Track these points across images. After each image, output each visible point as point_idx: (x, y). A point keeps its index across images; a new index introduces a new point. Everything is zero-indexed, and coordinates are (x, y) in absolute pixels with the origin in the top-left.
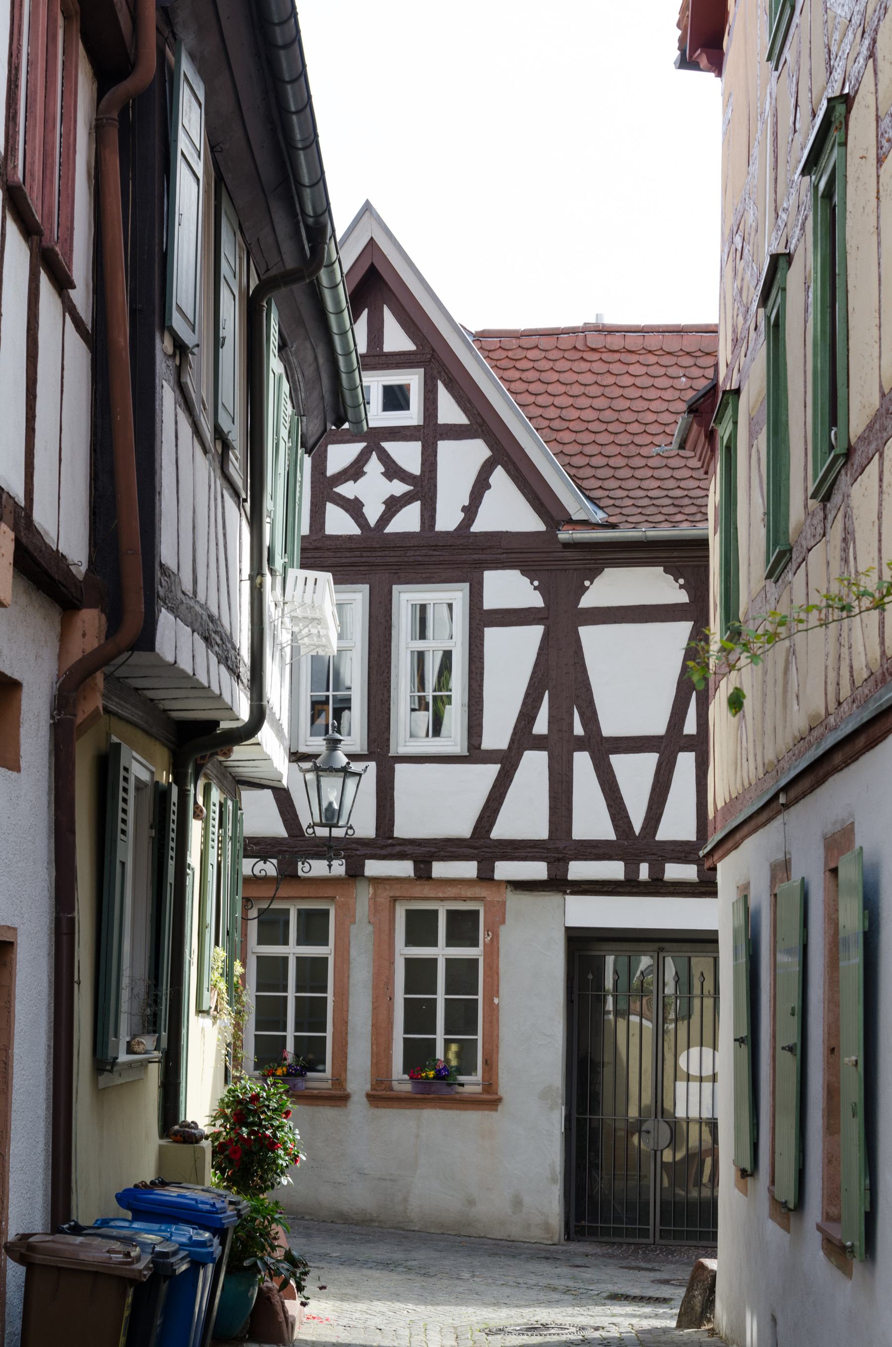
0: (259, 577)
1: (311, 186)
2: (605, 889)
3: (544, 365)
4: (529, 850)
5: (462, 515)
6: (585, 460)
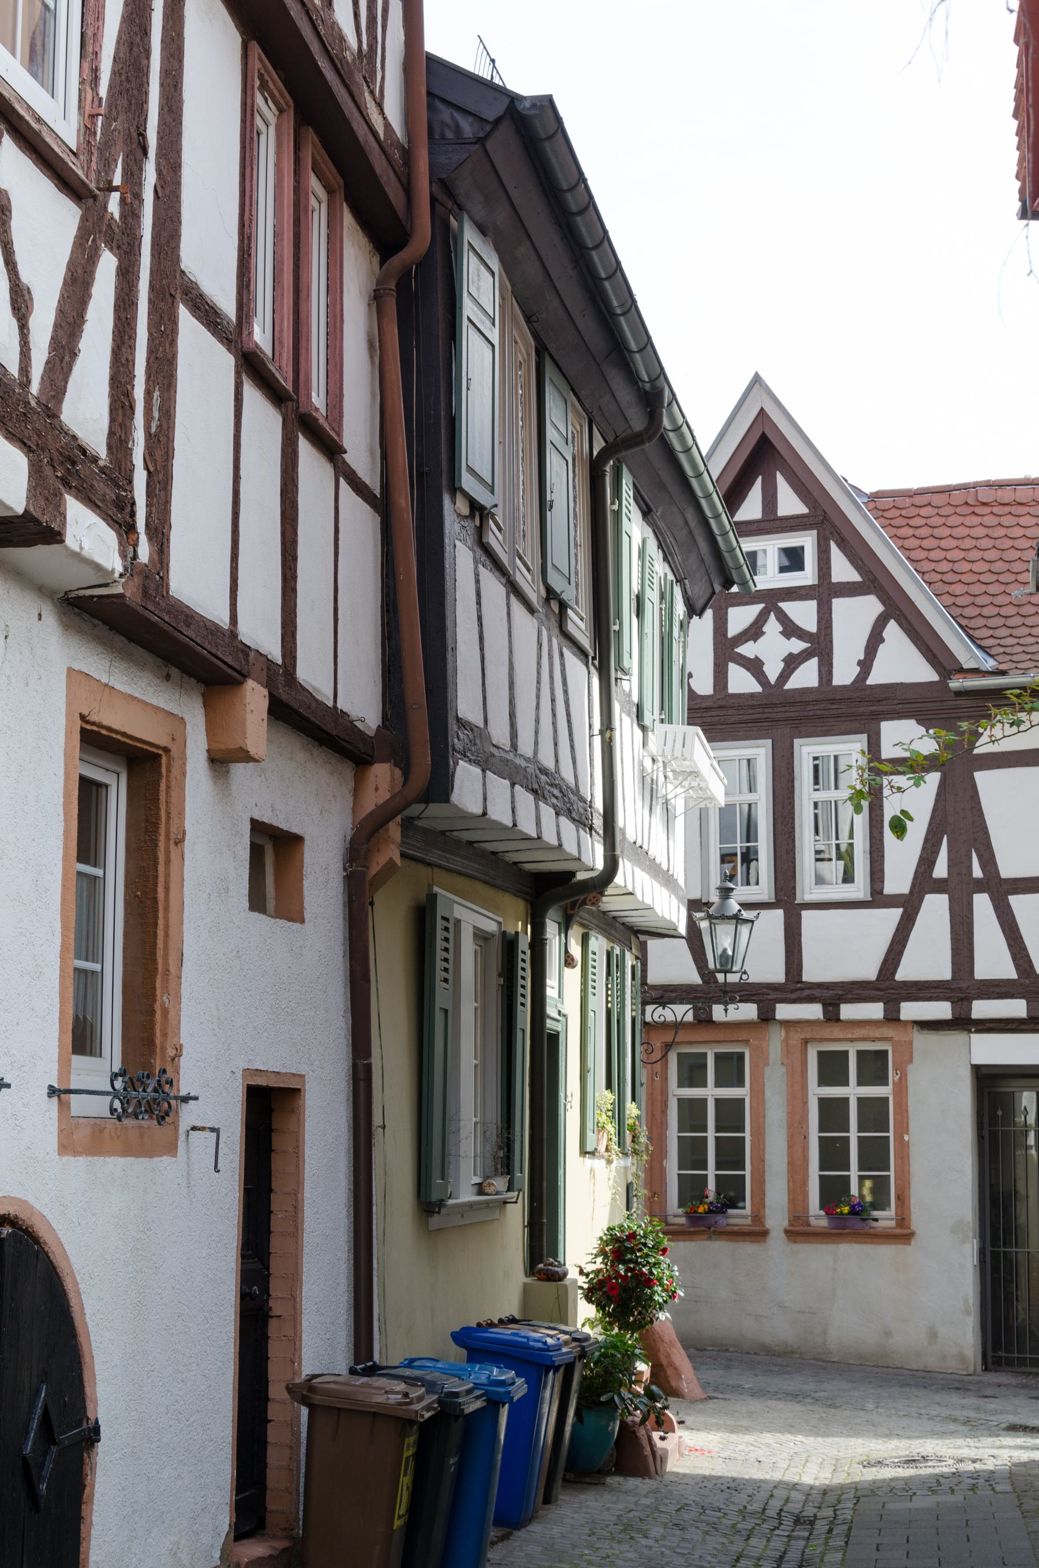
0: (608, 731)
1: (640, 351)
2: (1009, 1027)
3: (937, 521)
4: (933, 991)
5: (858, 669)
6: (977, 611)
